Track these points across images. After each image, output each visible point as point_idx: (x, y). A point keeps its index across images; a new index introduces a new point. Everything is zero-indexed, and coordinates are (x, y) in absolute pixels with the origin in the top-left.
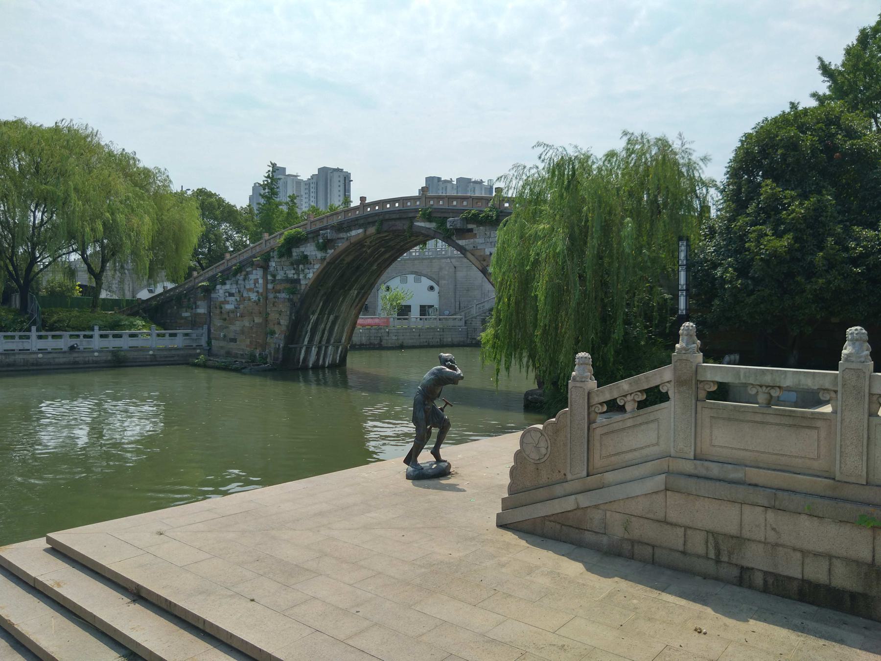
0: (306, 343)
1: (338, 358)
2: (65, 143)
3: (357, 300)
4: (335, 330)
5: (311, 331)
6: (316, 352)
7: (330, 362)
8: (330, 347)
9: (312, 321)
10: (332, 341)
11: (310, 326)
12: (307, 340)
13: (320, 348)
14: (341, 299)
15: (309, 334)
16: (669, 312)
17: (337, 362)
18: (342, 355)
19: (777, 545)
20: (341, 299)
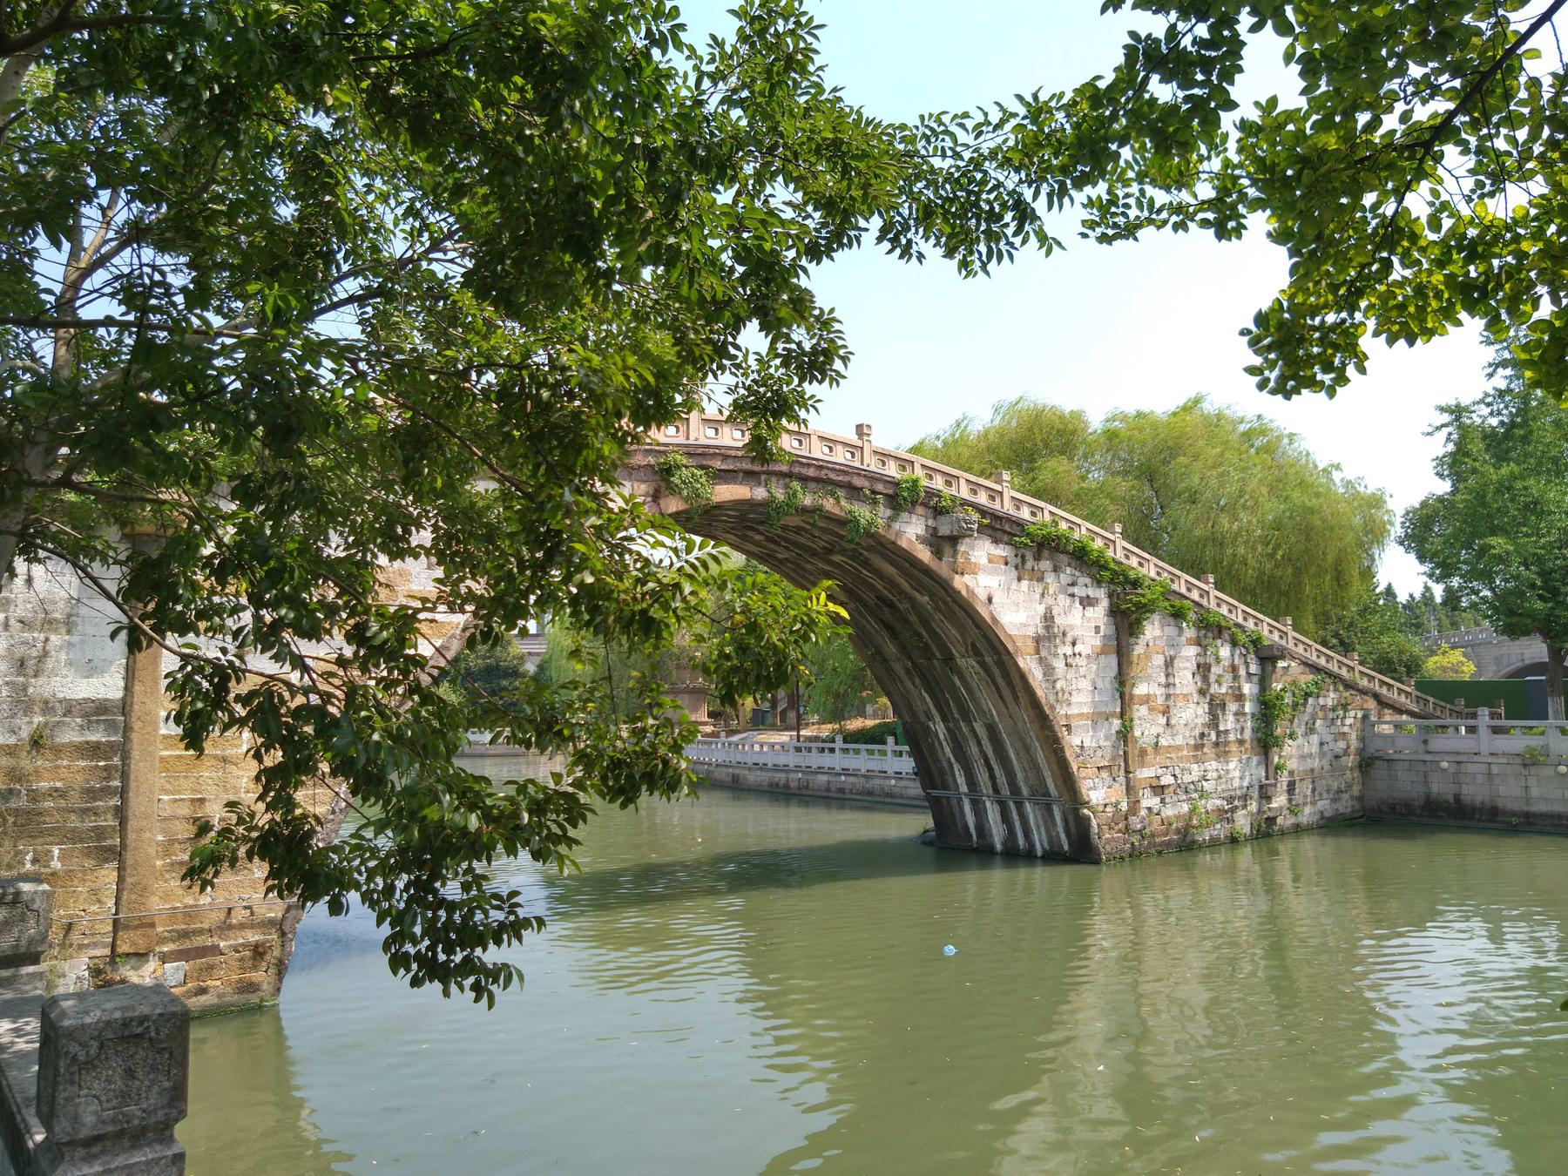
0: (964, 788)
1: (1063, 836)
2: (1105, 774)
3: (1000, 681)
4: (1013, 756)
5: (957, 760)
6: (999, 817)
7: (1046, 846)
8: (1028, 806)
9: (942, 737)
10: (1025, 791)
11: (947, 750)
12: (961, 780)
13: (1002, 805)
14: (958, 683)
15: (956, 767)
16: (435, 429)
17: (1066, 847)
18: (1073, 830)
19: (116, 922)
20: (958, 683)
